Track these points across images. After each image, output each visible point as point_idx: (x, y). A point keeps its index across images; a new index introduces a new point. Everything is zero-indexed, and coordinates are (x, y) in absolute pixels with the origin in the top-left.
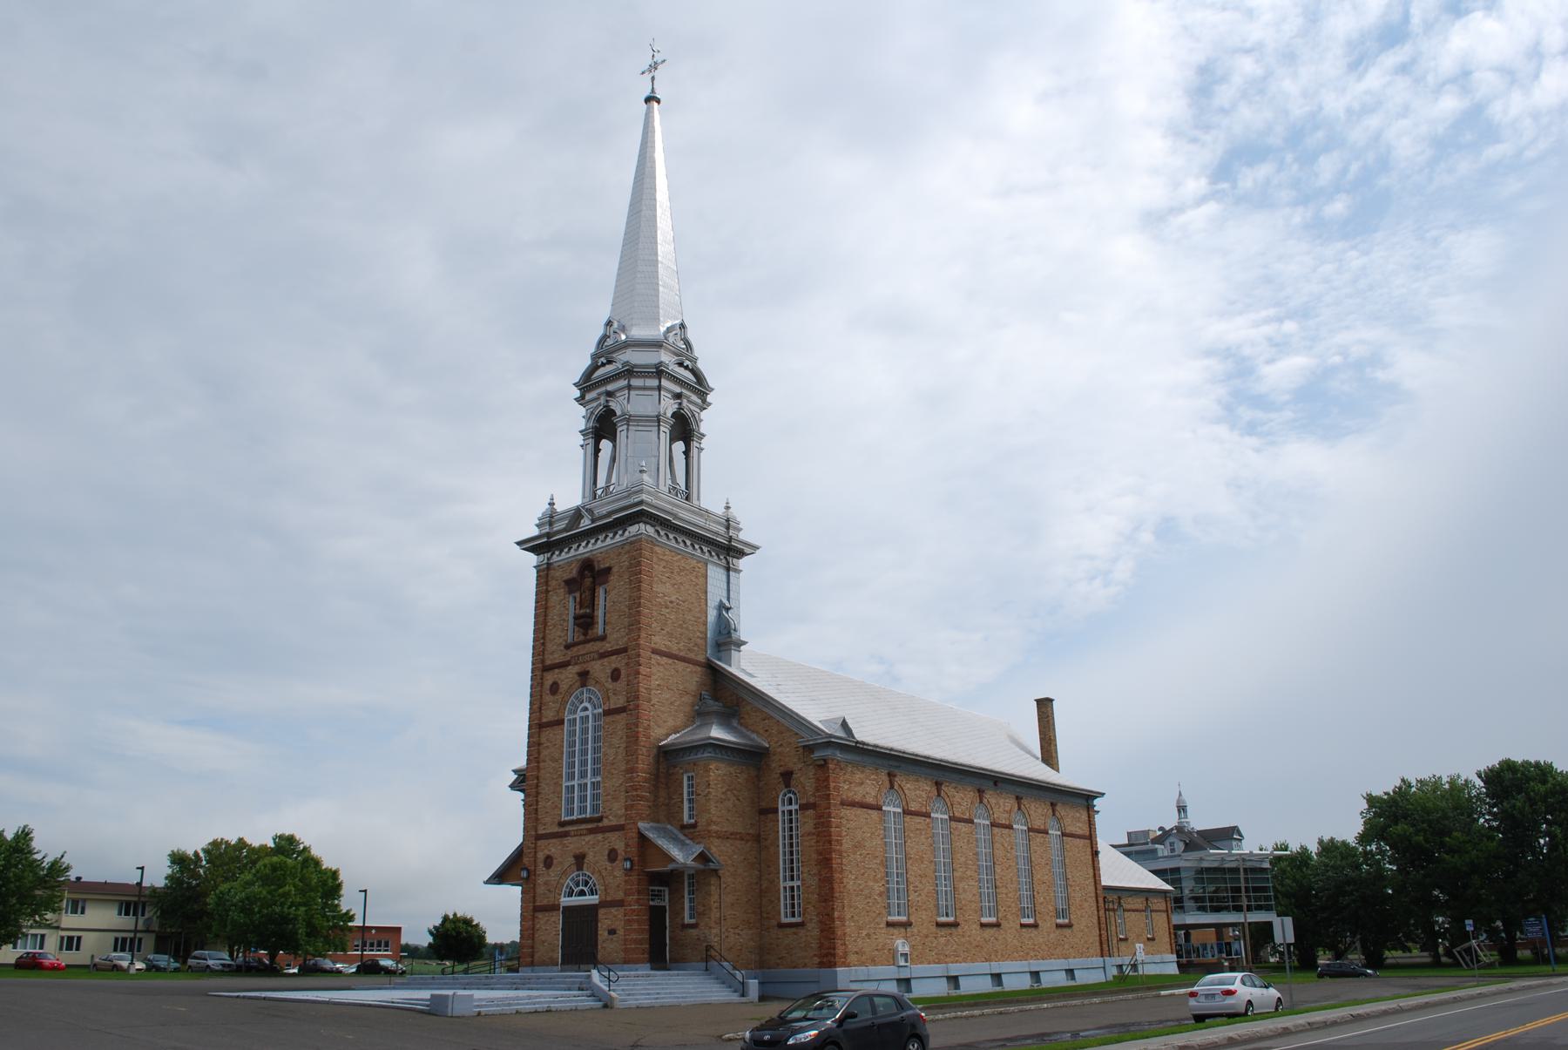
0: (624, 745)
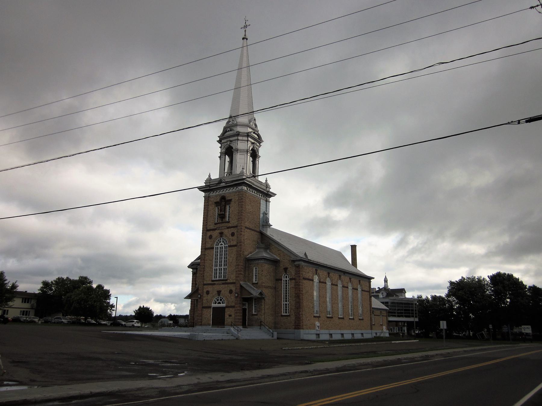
0: (235, 257)
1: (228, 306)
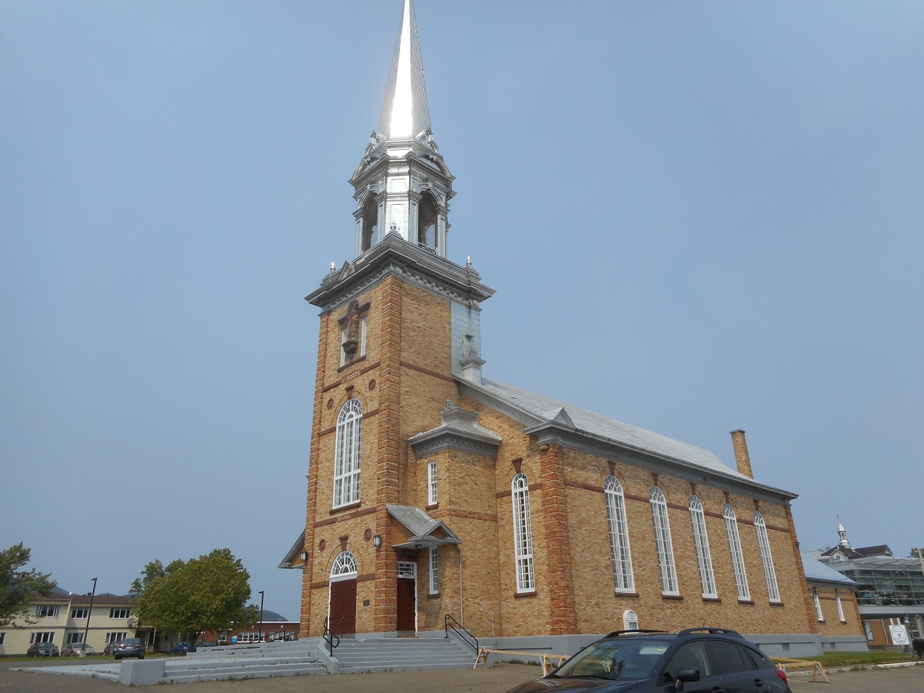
0: (377, 441)
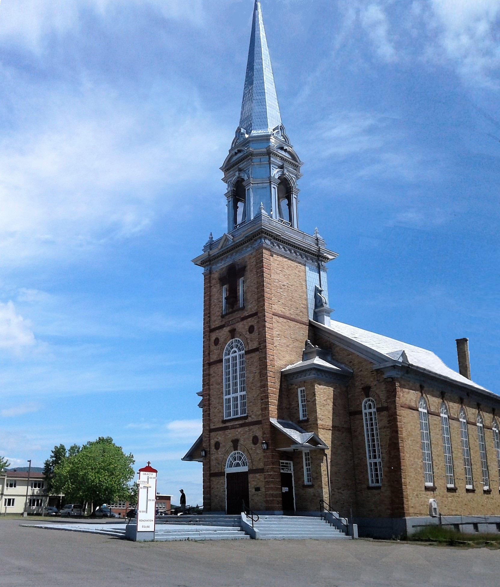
1: (253, 470)
